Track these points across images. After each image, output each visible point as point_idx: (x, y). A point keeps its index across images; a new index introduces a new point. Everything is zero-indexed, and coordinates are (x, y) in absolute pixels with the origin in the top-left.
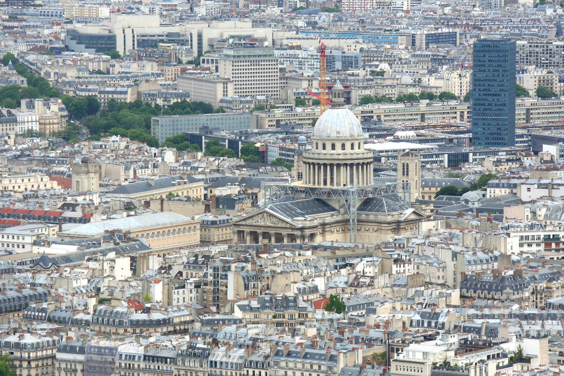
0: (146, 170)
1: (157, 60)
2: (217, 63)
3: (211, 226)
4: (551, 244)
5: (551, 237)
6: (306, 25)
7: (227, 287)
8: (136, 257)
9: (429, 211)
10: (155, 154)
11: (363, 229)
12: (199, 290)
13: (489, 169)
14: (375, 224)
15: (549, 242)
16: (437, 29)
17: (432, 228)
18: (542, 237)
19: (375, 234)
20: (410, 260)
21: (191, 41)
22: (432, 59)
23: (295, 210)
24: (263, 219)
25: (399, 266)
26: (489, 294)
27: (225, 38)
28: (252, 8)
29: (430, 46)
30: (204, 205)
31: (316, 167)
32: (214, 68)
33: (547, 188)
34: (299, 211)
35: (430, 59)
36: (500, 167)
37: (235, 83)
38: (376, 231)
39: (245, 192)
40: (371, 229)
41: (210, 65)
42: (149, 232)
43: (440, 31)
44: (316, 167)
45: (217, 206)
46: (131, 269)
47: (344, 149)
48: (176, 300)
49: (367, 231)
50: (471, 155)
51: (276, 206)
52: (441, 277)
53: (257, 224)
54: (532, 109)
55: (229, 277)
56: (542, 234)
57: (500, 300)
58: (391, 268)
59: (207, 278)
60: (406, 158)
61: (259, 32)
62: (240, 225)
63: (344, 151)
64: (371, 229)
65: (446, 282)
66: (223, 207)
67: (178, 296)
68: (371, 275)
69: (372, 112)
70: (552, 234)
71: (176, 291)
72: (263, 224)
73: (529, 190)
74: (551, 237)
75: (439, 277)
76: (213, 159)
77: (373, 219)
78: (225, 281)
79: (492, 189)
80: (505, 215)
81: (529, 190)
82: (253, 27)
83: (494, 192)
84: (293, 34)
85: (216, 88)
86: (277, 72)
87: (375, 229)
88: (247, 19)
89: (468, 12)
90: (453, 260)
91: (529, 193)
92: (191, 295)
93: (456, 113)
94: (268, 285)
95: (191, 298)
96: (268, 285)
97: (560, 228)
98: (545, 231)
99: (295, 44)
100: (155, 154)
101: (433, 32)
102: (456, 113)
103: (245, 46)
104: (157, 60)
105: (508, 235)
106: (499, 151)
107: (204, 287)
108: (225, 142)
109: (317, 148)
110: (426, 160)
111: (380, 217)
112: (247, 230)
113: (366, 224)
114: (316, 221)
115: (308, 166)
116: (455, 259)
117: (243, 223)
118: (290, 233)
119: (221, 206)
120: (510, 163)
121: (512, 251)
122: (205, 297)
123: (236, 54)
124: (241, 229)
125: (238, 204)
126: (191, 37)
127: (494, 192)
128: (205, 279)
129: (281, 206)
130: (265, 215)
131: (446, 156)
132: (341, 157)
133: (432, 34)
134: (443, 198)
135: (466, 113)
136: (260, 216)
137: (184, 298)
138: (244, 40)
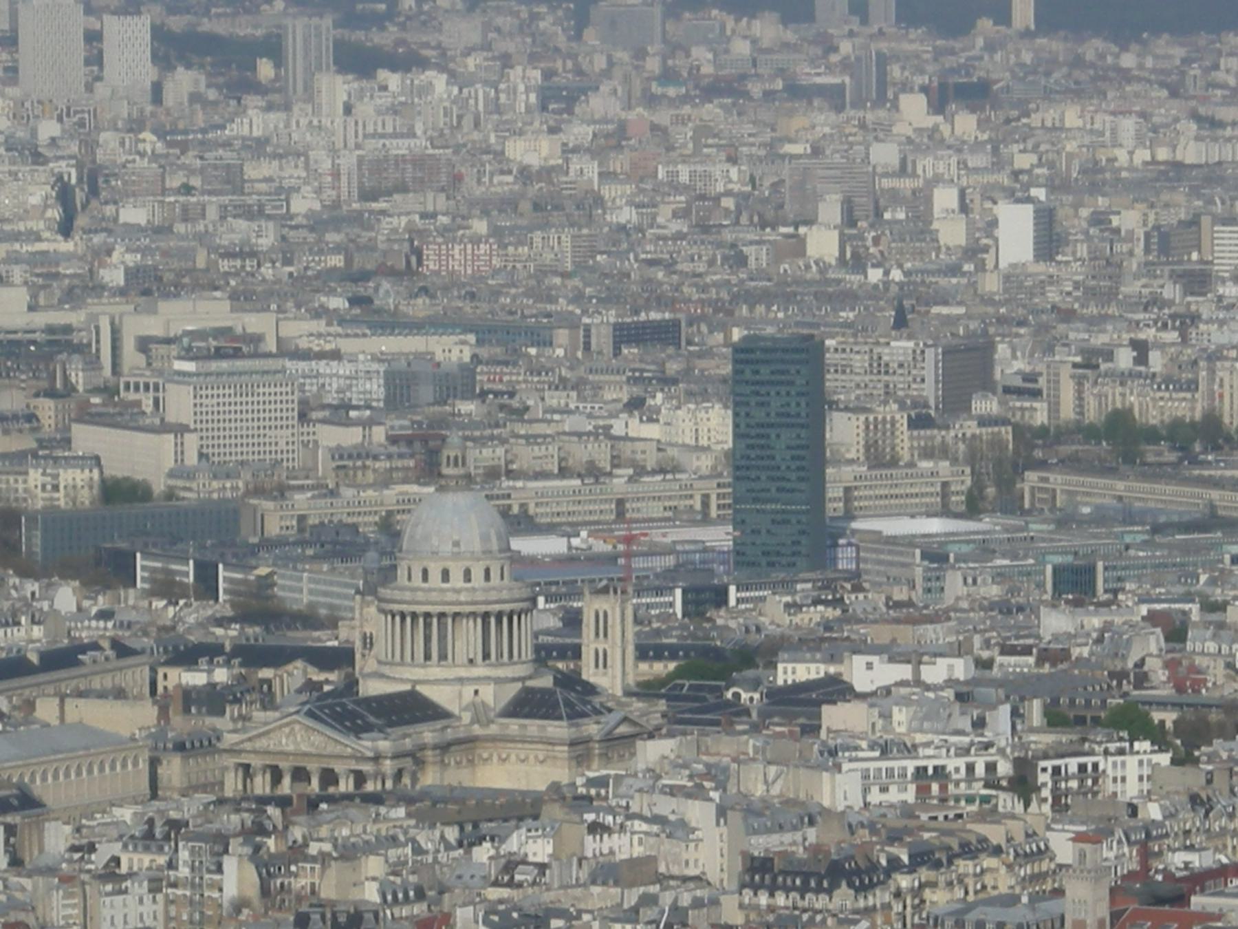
0: (15, 629)
1: (23, 385)
2: (156, 389)
3: (514, 726)
4: (929, 787)
5: (930, 771)
6: (347, 305)
7: (221, 890)
8: (15, 826)
9: (659, 715)
10: (33, 594)
11: (513, 757)
12: (160, 897)
13: (777, 621)
14: (540, 746)
15: (924, 783)
16: (637, 313)
17: (667, 752)
18: (910, 771)
19: (539, 768)
20: (622, 826)
21: (98, 342)
22: (629, 379)
23: (362, 717)
24: (291, 738)
25: (598, 837)
26: (803, 898)
27: (172, 335)
28: (226, 269)
29: (625, 351)
30: (156, 708)
31: (409, 620)
32: (151, 402)
33: (909, 662)
34: (372, 719)
35: (624, 378)
36: (800, 616)
37: (200, 434)
38: (542, 762)
39: (242, 678)
40: (532, 757)
41: (140, 396)
42: (35, 767)
43: (643, 317)
44: (409, 620)
45: (187, 710)
46: (6, 851)
47: (469, 580)
48: (109, 919)
49: (523, 761)
50: (732, 589)
51: (321, 708)
52: (691, 863)
53: (279, 749)
54: (856, 488)
55: (225, 867)
56: (911, 765)
57: (828, 911)
58: (582, 844)
59: (176, 869)
60: (602, 597)
61: (254, 322)
62: (240, 752)
63: (468, 585)
64: (532, 757)
65: (704, 873)
66: (199, 712)
67: (113, 912)
68: (539, 859)
69: (509, 496)
70: (930, 764)
71: (108, 900)
72: (291, 748)
73: (869, 666)
74: (930, 771)
75: (687, 863)
76: (164, 603)
77: (536, 734)
78: (217, 877)
79: (790, 666)
80: (826, 722)
81: (869, 666)
82: (232, 311)
83: (794, 673)
84: (320, 326)
85: (700, 394)
86: (293, 410)
87: (541, 757)
88: (218, 294)
89: (700, 275)
90: (718, 824)
91: (869, 672)
92: (141, 909)
93: (691, 497)
94: (313, 885)
95: (141, 916)
96: (313, 885)
97: (948, 751)
98: (916, 758)
99: (328, 347)
100: (33, 594)
101: (629, 320)
102: (691, 497)
103: (219, 354)
104: (23, 385)
105: (838, 768)
106: (797, 582)
107: (170, 891)
108: (188, 564)
109: (410, 578)
110: (662, 599)
111: (550, 729)
112: (256, 762)
113: (520, 745)
114: (407, 740)
115: (389, 618)
116: (722, 821)
117: (248, 746)
118: (353, 768)
119: (193, 710)
120: (820, 608)
121: (848, 803)
122: (173, 913)
123: (202, 370)
124: (244, 760)
125: (784, 661)
126: (98, 333)
127: (794, 673)
128: (171, 873)
129: (331, 707)
130: (297, 727)
131: (678, 592)
132: (462, 598)
133: (629, 324)
134: (682, 686)
135: (713, 497)
136: (287, 730)
137: (125, 916)
138: (215, 338)
